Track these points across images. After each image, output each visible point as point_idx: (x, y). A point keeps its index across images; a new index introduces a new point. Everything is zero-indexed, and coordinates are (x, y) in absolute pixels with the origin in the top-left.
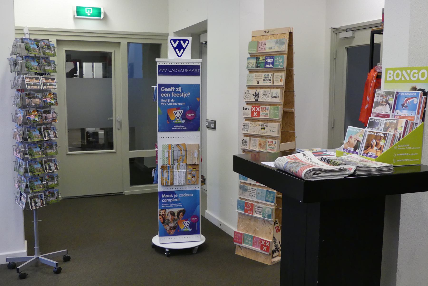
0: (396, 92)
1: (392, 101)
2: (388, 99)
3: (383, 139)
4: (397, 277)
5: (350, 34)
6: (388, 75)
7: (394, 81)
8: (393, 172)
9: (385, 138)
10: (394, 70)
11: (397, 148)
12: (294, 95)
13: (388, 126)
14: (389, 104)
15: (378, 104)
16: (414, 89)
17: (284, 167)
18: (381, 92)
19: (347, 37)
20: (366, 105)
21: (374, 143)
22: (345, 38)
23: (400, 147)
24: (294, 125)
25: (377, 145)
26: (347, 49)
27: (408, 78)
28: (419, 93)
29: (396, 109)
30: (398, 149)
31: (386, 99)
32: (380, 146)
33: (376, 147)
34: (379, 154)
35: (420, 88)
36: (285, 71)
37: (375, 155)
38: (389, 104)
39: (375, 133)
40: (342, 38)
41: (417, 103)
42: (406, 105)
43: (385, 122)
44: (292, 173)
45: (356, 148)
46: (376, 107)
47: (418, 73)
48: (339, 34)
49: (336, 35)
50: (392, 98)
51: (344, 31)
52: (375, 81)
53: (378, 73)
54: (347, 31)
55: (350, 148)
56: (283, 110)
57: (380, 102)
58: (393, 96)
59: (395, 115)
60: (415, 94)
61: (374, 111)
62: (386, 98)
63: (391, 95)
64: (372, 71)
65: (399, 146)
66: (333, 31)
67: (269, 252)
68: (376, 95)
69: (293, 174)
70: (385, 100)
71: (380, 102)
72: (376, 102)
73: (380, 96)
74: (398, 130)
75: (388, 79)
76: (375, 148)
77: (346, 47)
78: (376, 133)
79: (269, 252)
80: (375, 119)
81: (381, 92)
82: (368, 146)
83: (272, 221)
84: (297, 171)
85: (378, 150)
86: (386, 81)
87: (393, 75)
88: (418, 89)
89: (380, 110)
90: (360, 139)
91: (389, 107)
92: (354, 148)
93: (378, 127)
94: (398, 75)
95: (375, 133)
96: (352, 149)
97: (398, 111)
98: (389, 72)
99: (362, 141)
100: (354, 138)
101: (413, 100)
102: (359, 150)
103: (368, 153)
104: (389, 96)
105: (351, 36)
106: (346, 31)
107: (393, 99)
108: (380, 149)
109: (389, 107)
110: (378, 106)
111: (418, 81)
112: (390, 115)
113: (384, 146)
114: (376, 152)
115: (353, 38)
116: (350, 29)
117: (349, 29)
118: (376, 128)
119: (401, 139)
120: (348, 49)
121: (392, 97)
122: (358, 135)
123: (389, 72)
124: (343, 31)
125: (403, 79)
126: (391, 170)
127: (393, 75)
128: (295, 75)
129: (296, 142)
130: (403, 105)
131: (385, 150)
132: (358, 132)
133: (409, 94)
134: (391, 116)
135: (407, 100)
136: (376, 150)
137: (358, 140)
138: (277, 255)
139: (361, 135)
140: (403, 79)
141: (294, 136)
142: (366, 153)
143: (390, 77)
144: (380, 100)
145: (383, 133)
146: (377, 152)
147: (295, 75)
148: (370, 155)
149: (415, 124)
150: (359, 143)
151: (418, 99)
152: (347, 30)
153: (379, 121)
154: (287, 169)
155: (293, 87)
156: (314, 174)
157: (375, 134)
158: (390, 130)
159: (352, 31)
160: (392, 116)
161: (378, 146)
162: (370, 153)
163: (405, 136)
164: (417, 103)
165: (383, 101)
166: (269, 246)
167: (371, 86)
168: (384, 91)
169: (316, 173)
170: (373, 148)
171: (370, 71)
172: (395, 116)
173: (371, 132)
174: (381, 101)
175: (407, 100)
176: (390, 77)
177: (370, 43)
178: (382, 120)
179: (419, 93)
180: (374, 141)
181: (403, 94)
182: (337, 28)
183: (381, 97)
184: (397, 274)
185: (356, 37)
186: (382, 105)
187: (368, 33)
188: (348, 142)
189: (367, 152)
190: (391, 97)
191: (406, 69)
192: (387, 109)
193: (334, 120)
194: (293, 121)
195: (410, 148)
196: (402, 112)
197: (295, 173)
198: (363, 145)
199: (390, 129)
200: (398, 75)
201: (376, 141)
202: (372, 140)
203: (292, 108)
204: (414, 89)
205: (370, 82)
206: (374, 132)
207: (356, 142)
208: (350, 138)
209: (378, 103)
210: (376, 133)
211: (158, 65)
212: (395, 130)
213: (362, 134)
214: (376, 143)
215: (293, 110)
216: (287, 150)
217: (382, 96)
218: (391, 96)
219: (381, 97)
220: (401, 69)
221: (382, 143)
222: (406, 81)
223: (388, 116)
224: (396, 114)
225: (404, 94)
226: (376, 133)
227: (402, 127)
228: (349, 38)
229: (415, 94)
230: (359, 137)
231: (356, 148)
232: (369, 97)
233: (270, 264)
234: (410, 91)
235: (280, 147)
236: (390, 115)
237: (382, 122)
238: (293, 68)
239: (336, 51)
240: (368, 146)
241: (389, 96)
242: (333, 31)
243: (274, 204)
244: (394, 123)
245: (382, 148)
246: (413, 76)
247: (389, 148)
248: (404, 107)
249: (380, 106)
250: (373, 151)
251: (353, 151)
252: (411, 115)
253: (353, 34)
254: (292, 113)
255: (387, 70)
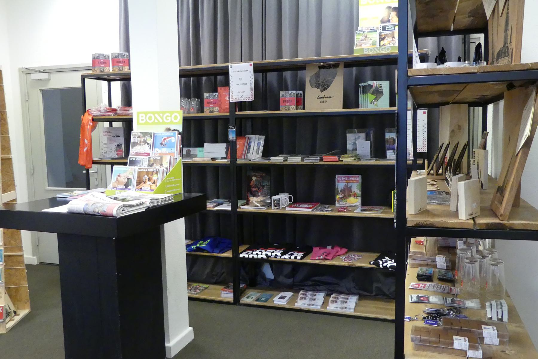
0: (154, 133)
1: (151, 141)
2: (146, 139)
3: (156, 174)
4: (168, 294)
5: (44, 76)
6: (141, 118)
7: (146, 123)
8: (173, 201)
9: (157, 173)
10: (146, 113)
11: (167, 181)
12: (9, 140)
13: (152, 163)
14: (148, 144)
15: (135, 144)
16: (169, 130)
17: (84, 209)
18: (138, 133)
19: (41, 79)
20: (84, 148)
21: (146, 179)
22: (39, 79)
23: (169, 180)
24: (13, 173)
25: (149, 180)
26: (41, 91)
27: (162, 121)
28: (175, 133)
29: (155, 148)
30: (168, 181)
31: (144, 140)
32: (154, 180)
33: (150, 182)
34: (154, 187)
35: (175, 129)
36: (202, 111)
37: (150, 189)
38: (148, 144)
39: (145, 170)
40: (34, 79)
41: (175, 142)
42: (164, 143)
43: (148, 160)
44: (98, 213)
45: (127, 185)
46: (134, 147)
47: (171, 116)
48: (31, 75)
49: (25, 77)
50: (151, 138)
51: (37, 72)
52: (91, 124)
53: (94, 116)
54: (40, 72)
55: (119, 186)
56: (1, 157)
57: (137, 142)
58: (151, 136)
59: (154, 153)
60: (172, 134)
61: (132, 150)
62: (143, 139)
63: (149, 136)
64: (86, 114)
65: (168, 179)
66: (22, 71)
67: (3, 319)
68: (133, 136)
69: (100, 214)
70: (143, 140)
71: (137, 142)
72: (133, 142)
73: (136, 137)
74: (163, 165)
75: (141, 122)
76: (148, 183)
77: (40, 90)
78: (147, 170)
79: (3, 319)
80: (135, 158)
81: (138, 133)
82: (140, 182)
83: (2, 283)
84: (105, 210)
85: (152, 184)
86: (138, 123)
87: (146, 118)
88: (172, 129)
89: (139, 149)
90: (131, 176)
91: (149, 146)
92: (125, 185)
93: (140, 165)
94: (150, 118)
95: (145, 170)
96: (124, 187)
97: (156, 149)
98: (141, 115)
99: (133, 178)
100: (123, 177)
101: (171, 139)
102: (131, 186)
103: (141, 188)
104: (146, 137)
105: (47, 78)
106: (39, 73)
107: (151, 138)
108: (154, 183)
109: (149, 146)
110: (136, 146)
111: (171, 122)
112: (150, 153)
113: (157, 180)
114: (150, 186)
115: (48, 80)
116: (44, 71)
117: (43, 71)
118: (138, 166)
119: (168, 173)
120: (43, 91)
121: (150, 137)
122: (127, 173)
123: (141, 115)
124: (36, 72)
125: (156, 121)
126: (171, 199)
127: (146, 118)
128: (8, 118)
129: (17, 191)
130: (161, 144)
131: (159, 183)
132: (127, 171)
133: (166, 134)
134: (151, 154)
135: (165, 139)
136: (150, 184)
137: (128, 177)
138: (9, 320)
139: (131, 172)
140: (156, 121)
141: (14, 185)
142: (139, 188)
143: (142, 120)
144: (138, 140)
145: (154, 169)
146: (151, 187)
147: (8, 118)
148: (144, 189)
149: (175, 159)
150: (130, 180)
151: (175, 138)
152: (40, 71)
153: (140, 159)
154: (90, 211)
155: (8, 131)
156: (123, 210)
157: (146, 171)
158: (155, 166)
159: (47, 73)
160: (152, 154)
161: (151, 180)
162: (144, 187)
163: (170, 171)
164: (175, 142)
165: (141, 141)
166: (2, 312)
167: (88, 129)
168: (141, 132)
169: (124, 209)
170: (146, 183)
171: (84, 115)
172: (154, 154)
173: (141, 169)
174: (139, 141)
175: (165, 139)
176: (142, 120)
177: (81, 86)
178: (143, 158)
179: (175, 133)
180: (146, 176)
181: (160, 134)
182: (29, 68)
183: (138, 138)
184: (167, 292)
185: (52, 79)
186: (140, 144)
187: (78, 75)
188: (117, 180)
189: (140, 187)
190: (149, 138)
191: (158, 113)
192: (146, 148)
193: (33, 166)
194: (11, 169)
195: (174, 180)
196: (161, 150)
197: (103, 212)
198: (134, 182)
199: (155, 165)
200: (150, 118)
201: (148, 176)
202: (144, 176)
203: (8, 155)
204: (169, 130)
205: (86, 125)
206: (144, 169)
207: (126, 180)
208: (119, 177)
209: (136, 143)
210: (147, 170)
211: (396, 107)
212: (160, 166)
213: (132, 172)
214: (149, 178)
215: (10, 156)
216: (7, 202)
217: (139, 137)
218: (148, 136)
219: (138, 138)
220: (154, 113)
221: (155, 177)
222: (159, 123)
223: (148, 154)
224: (155, 152)
225: (161, 134)
226: (146, 170)
227: (167, 162)
228: (42, 80)
229: (172, 134)
230: (129, 175)
231: (127, 185)
232: (87, 140)
233: (4, 332)
234: (165, 131)
235: (1, 198)
236: (150, 153)
237: (144, 160)
238: (6, 110)
239: (28, 92)
240: (140, 182)
241: (146, 137)
242: (22, 71)
243: (3, 262)
244: (158, 159)
245: (156, 181)
246: (166, 118)
247: (161, 182)
248: (162, 146)
249: (138, 146)
250: (147, 186)
251: (124, 188)
252: (171, 152)
253: (49, 76)
254: (10, 160)
255: (138, 113)
